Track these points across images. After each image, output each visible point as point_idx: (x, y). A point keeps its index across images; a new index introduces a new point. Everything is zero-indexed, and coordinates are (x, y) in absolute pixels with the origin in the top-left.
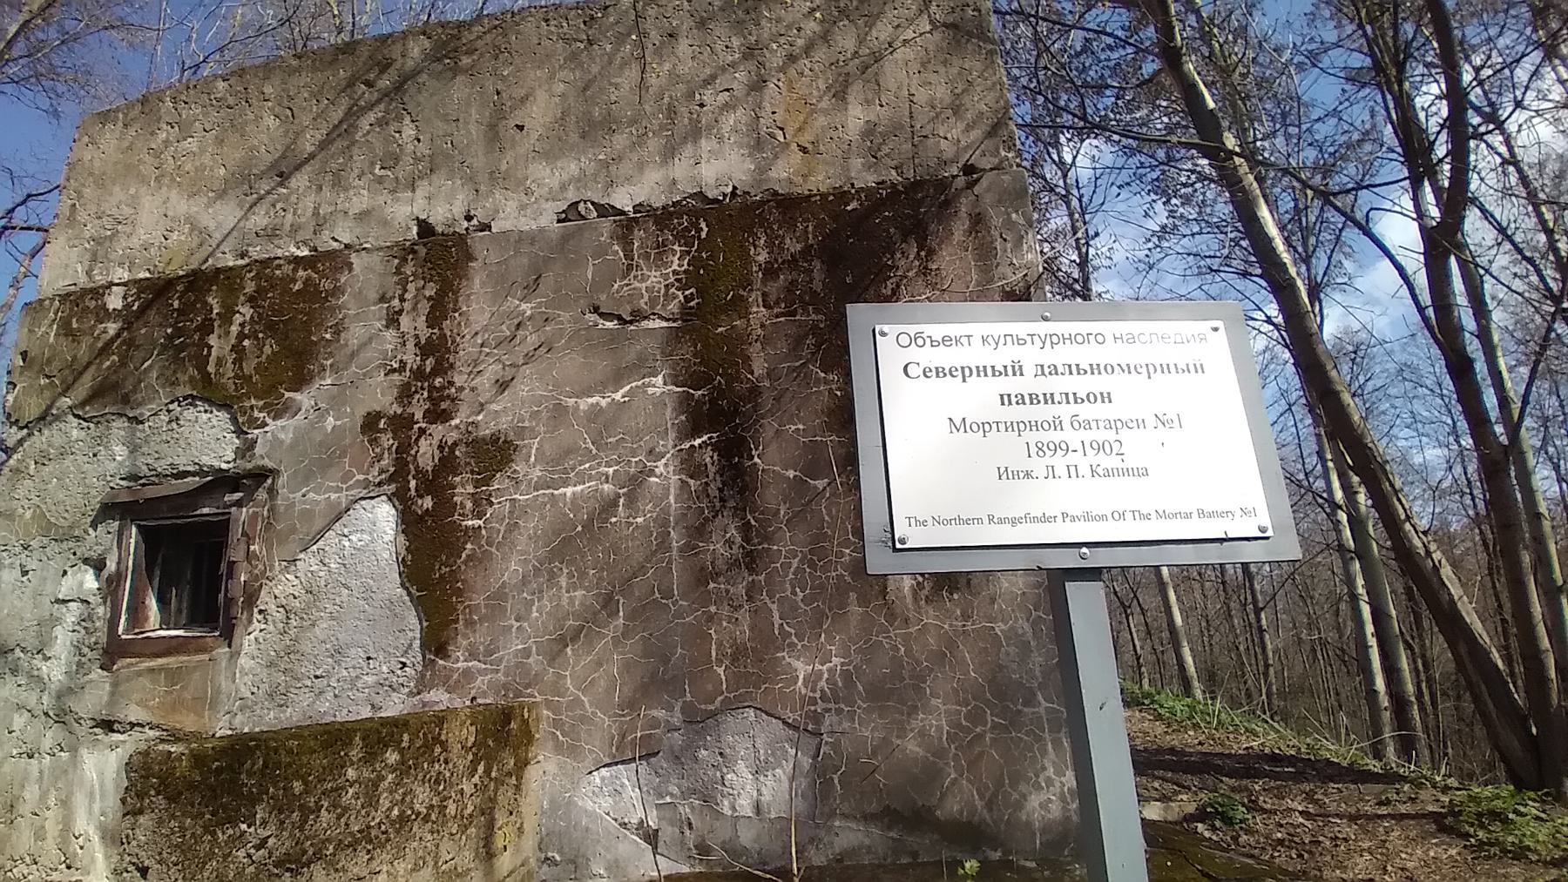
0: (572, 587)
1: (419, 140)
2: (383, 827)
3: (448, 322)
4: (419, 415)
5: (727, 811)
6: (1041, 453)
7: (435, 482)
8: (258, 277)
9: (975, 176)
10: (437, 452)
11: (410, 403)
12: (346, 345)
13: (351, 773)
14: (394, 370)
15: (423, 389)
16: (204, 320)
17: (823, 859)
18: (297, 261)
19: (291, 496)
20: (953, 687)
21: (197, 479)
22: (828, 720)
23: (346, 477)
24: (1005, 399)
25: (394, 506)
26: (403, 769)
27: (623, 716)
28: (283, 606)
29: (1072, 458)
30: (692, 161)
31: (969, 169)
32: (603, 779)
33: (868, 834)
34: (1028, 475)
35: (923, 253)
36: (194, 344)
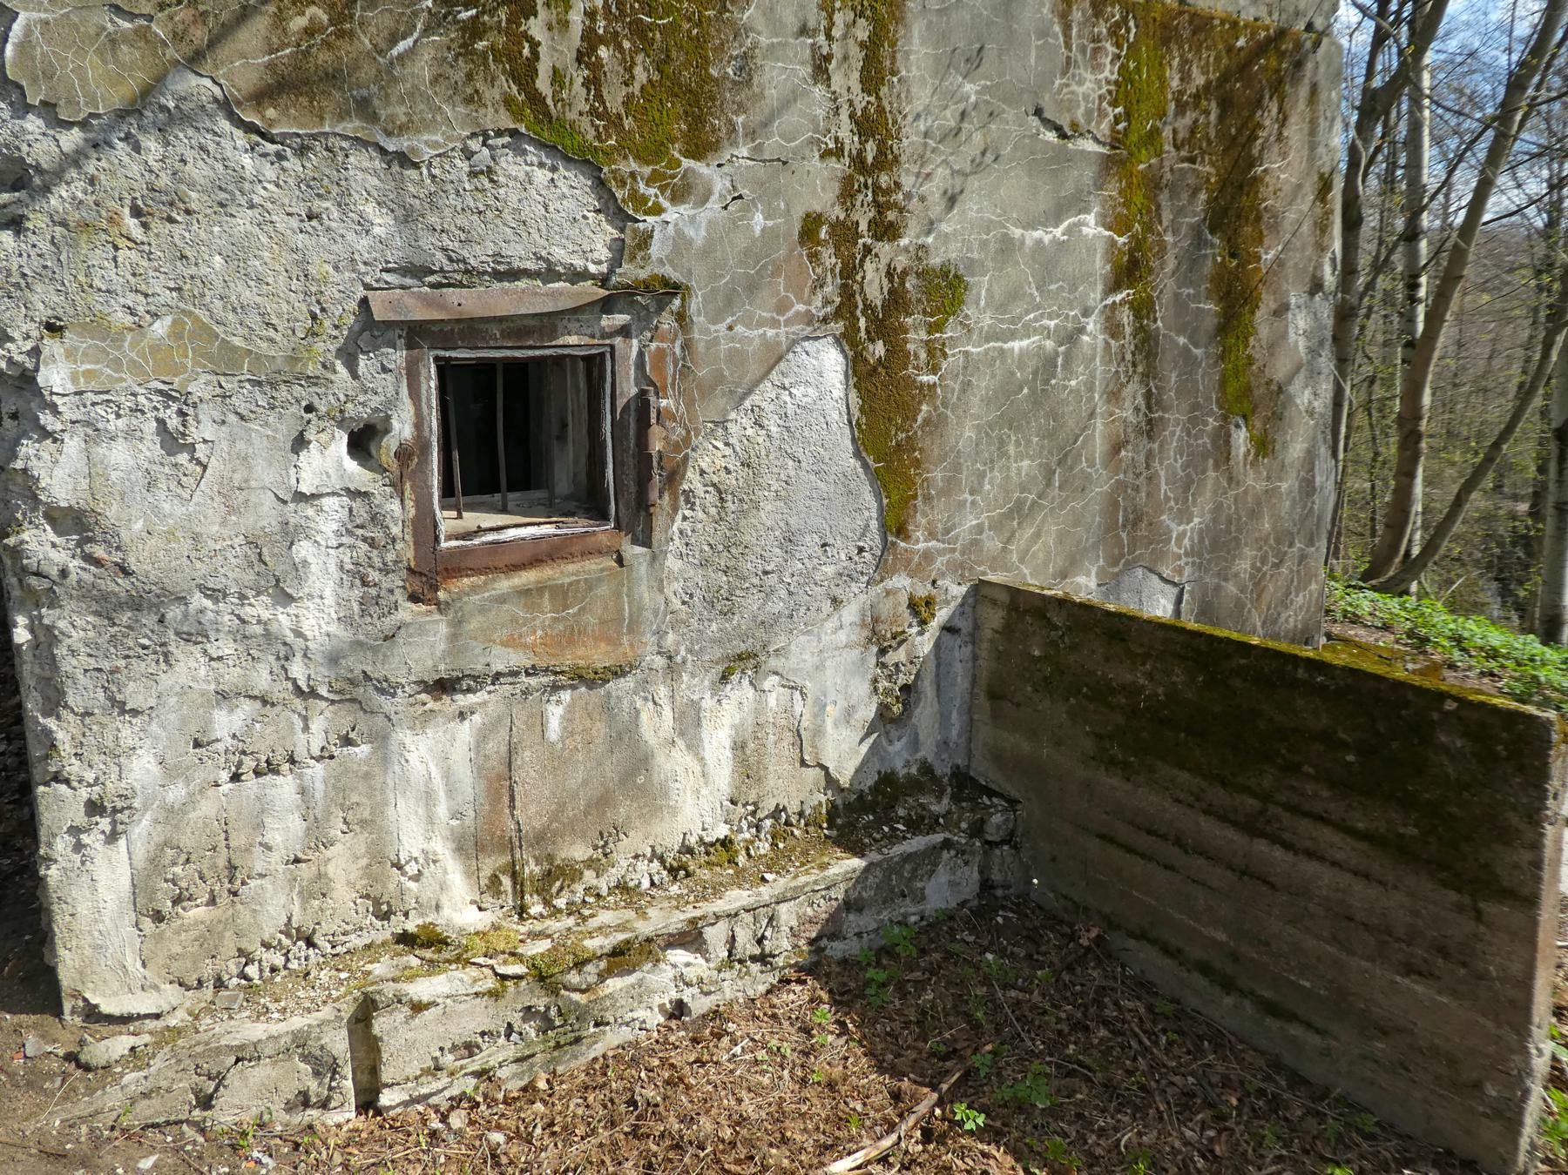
0: (1020, 457)
4: (863, 227)
7: (886, 324)
10: (885, 282)
12: (762, 96)
19: (713, 328)
23: (782, 307)
25: (843, 351)
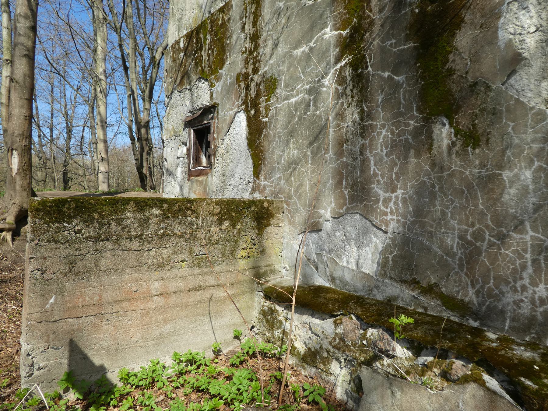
17: (382, 297)
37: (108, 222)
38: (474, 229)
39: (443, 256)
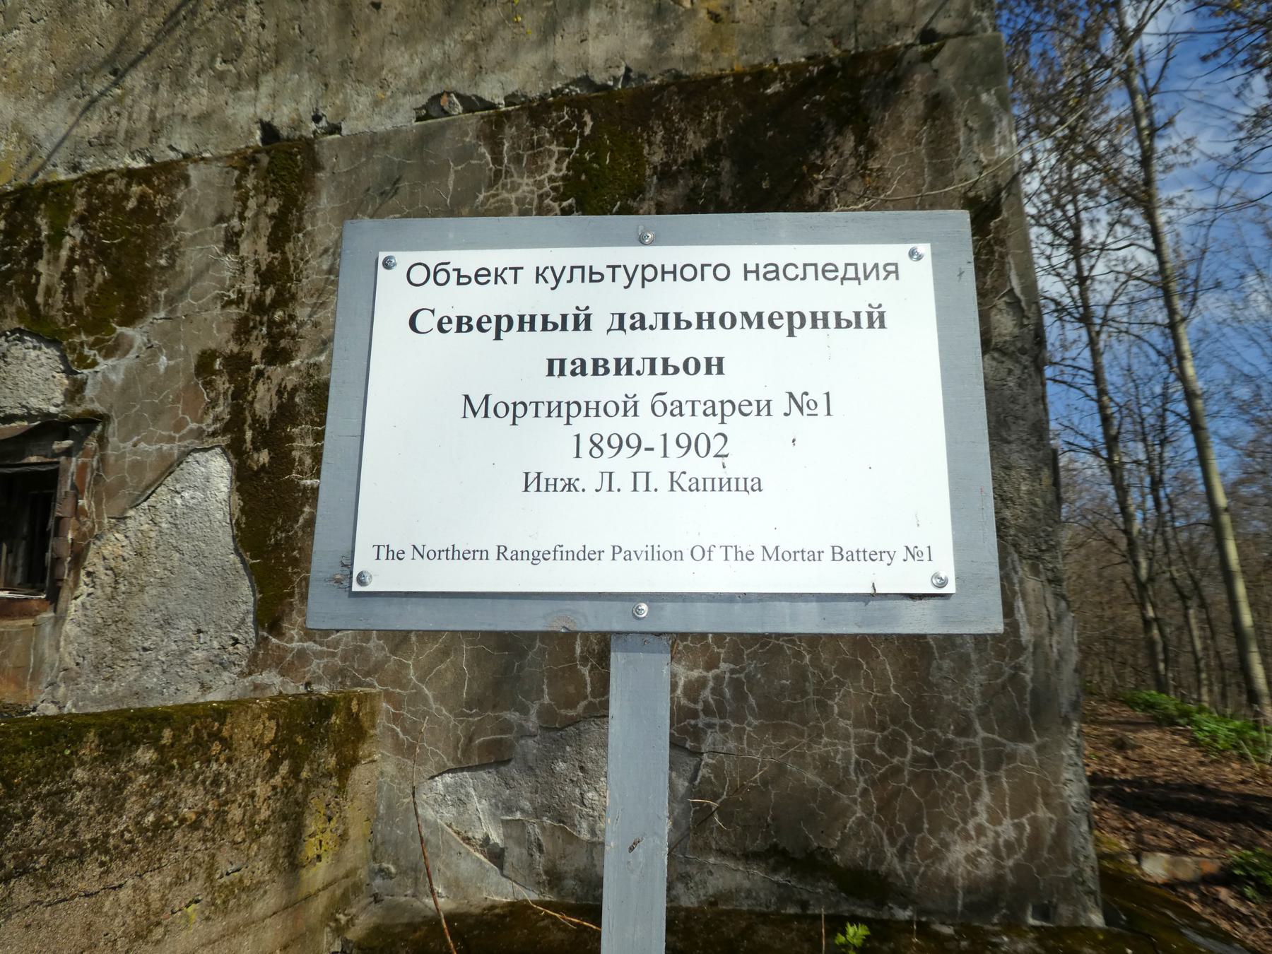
1: (263, 26)
2: (127, 836)
3: (291, 244)
4: (257, 355)
5: (585, 836)
6: (596, 452)
8: (89, 194)
9: (935, 44)
10: (275, 399)
11: (248, 340)
12: (182, 272)
13: (80, 774)
14: (230, 303)
15: (261, 324)
16: (32, 243)
17: (694, 900)
18: (130, 174)
19: (122, 445)
20: (867, 707)
21: (26, 423)
22: (710, 739)
23: (179, 426)
24: (555, 367)
25: (229, 461)
26: (162, 769)
27: (471, 716)
28: (111, 569)
29: (643, 461)
30: (577, 38)
31: (928, 36)
32: (446, 786)
33: (748, 875)
34: (570, 485)
35: (862, 149)
36: (21, 271)
37: (24, 809)
38: (886, 733)
39: (829, 791)
